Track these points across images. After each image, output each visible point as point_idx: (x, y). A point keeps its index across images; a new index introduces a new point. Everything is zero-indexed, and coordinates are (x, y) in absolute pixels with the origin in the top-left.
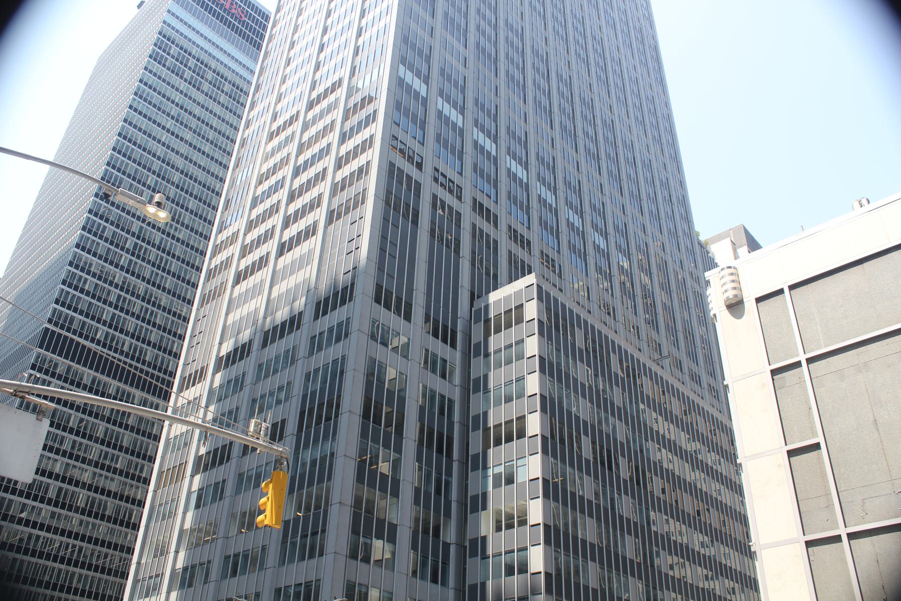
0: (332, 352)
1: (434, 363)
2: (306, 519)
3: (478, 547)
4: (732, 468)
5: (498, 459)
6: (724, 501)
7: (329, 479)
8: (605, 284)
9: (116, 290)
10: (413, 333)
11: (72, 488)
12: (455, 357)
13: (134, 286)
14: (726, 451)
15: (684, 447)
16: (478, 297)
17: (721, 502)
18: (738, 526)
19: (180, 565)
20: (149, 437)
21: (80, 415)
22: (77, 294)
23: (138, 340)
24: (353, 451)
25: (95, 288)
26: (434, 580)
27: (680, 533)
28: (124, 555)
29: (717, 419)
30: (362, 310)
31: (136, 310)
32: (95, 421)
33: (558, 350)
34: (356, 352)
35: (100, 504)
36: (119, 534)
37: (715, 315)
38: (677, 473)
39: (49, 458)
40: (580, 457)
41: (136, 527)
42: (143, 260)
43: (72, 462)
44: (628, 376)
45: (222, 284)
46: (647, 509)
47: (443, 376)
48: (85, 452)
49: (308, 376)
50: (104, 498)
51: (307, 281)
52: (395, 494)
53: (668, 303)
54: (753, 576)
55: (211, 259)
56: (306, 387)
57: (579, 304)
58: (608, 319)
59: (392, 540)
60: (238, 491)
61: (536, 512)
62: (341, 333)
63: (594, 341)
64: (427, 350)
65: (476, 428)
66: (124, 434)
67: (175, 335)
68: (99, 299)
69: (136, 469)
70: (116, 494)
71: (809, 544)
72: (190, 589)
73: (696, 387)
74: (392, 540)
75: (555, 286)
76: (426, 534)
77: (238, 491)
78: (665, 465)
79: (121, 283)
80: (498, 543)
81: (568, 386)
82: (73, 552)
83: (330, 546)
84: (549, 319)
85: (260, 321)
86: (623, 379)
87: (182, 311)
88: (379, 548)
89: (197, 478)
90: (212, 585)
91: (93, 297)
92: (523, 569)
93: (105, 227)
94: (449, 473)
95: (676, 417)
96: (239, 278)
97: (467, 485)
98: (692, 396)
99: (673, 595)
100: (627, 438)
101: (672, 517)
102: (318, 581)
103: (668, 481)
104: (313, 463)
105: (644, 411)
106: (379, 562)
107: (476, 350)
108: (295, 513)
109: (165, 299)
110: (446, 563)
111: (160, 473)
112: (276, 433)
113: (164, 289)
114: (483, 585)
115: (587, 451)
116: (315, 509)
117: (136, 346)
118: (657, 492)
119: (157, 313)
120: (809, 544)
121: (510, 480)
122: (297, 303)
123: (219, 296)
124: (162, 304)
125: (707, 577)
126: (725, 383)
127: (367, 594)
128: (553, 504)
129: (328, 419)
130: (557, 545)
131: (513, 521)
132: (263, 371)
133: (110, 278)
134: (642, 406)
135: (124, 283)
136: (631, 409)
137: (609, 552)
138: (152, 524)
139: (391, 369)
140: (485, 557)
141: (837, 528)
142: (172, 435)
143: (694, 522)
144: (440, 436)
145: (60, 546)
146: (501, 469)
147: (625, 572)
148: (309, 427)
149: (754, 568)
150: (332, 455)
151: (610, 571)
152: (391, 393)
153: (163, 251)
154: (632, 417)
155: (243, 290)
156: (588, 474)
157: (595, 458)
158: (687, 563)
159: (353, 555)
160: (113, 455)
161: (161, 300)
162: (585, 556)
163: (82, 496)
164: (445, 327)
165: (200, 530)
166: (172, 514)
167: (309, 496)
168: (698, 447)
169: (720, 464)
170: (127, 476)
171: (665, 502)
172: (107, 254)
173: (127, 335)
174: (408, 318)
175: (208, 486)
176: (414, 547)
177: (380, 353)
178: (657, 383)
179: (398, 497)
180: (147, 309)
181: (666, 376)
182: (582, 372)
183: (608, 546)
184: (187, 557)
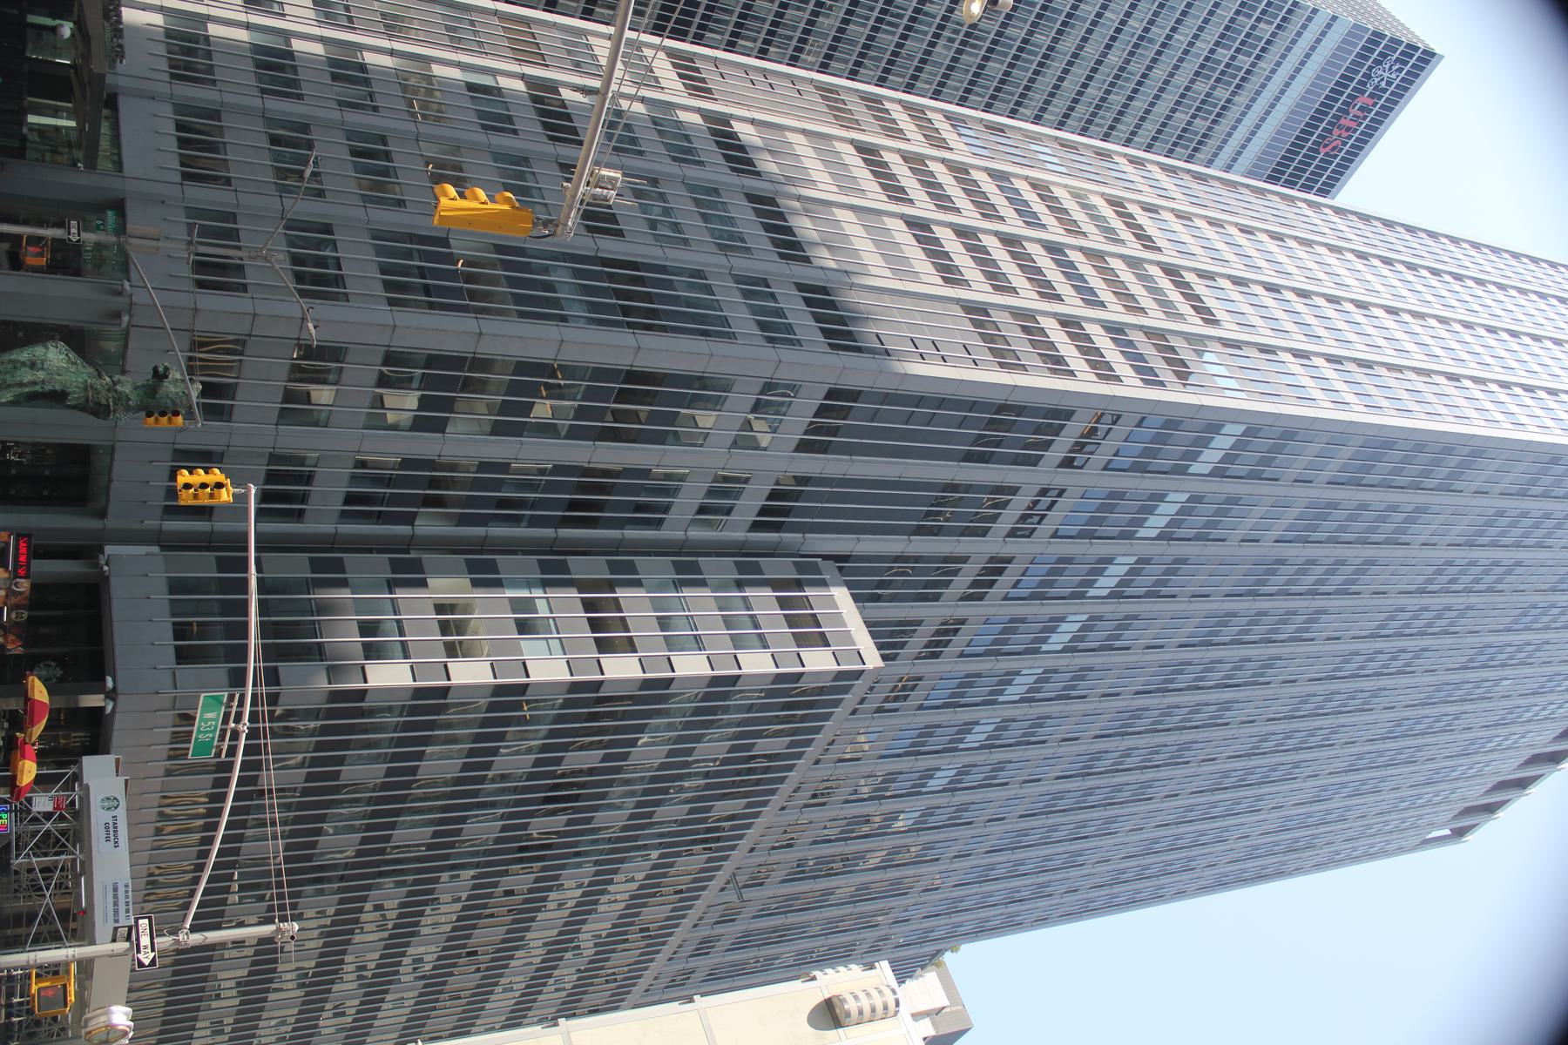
0: (740, 315)
1: (725, 494)
2: (453, 275)
3: (409, 573)
5: (560, 606)
7: (522, 314)
8: (865, 790)
10: (776, 456)
12: (736, 529)
14: (579, 1001)
15: (585, 928)
16: (840, 569)
19: (370, 58)
24: (571, 355)
26: (350, 499)
29: (634, 985)
30: (816, 366)
33: (750, 708)
34: (742, 357)
37: (814, 978)
38: (540, 916)
40: (565, 747)
44: (708, 830)
47: (703, 510)
49: (699, 274)
52: (498, 429)
53: (833, 899)
55: (900, 102)
56: (679, 272)
58: (804, 797)
59: (419, 425)
60: (498, 156)
61: (470, 673)
62: (775, 330)
64: (746, 481)
65: (614, 567)
67: (767, 42)
73: (688, 949)
74: (419, 425)
75: (862, 701)
76: (427, 484)
77: (498, 156)
78: (553, 895)
80: (415, 608)
84: (804, 693)
85: (793, 190)
88: (406, 402)
89: (519, 86)
90: (336, 115)
92: (373, 652)
94: (535, 522)
96: (866, 151)
97: (514, 553)
98: (673, 941)
99: (331, 911)
100: (600, 829)
101: (464, 909)
102: (346, 297)
104: (549, 287)
105: (646, 858)
106: (379, 402)
107: (747, 565)
110: (380, 518)
112: (599, 219)
113: (845, 21)
114: (343, 583)
115: (576, 760)
118: (506, 882)
121: (524, 627)
122: (825, 253)
124: (821, 19)
125: (364, 968)
126: (697, 997)
127: (325, 382)
129: (626, 311)
131: (454, 633)
132: (706, 197)
134: (655, 854)
140: (391, 585)
142: (592, 40)
143: (457, 946)
146: (543, 611)
147: (369, 828)
148: (611, 277)
150: (564, 319)
152: (672, 419)
154: (636, 838)
155: (848, 160)
156: (465, 767)
159: (390, 358)
161: (828, 16)
162: (395, 757)
164: (786, 512)
165: (430, 92)
166: (456, 43)
167: (492, 280)
171: (490, 896)
174: (803, 447)
176: (407, 463)
177: (741, 400)
178: (695, 881)
181: (708, 896)
182: (713, 748)
184: (382, 70)
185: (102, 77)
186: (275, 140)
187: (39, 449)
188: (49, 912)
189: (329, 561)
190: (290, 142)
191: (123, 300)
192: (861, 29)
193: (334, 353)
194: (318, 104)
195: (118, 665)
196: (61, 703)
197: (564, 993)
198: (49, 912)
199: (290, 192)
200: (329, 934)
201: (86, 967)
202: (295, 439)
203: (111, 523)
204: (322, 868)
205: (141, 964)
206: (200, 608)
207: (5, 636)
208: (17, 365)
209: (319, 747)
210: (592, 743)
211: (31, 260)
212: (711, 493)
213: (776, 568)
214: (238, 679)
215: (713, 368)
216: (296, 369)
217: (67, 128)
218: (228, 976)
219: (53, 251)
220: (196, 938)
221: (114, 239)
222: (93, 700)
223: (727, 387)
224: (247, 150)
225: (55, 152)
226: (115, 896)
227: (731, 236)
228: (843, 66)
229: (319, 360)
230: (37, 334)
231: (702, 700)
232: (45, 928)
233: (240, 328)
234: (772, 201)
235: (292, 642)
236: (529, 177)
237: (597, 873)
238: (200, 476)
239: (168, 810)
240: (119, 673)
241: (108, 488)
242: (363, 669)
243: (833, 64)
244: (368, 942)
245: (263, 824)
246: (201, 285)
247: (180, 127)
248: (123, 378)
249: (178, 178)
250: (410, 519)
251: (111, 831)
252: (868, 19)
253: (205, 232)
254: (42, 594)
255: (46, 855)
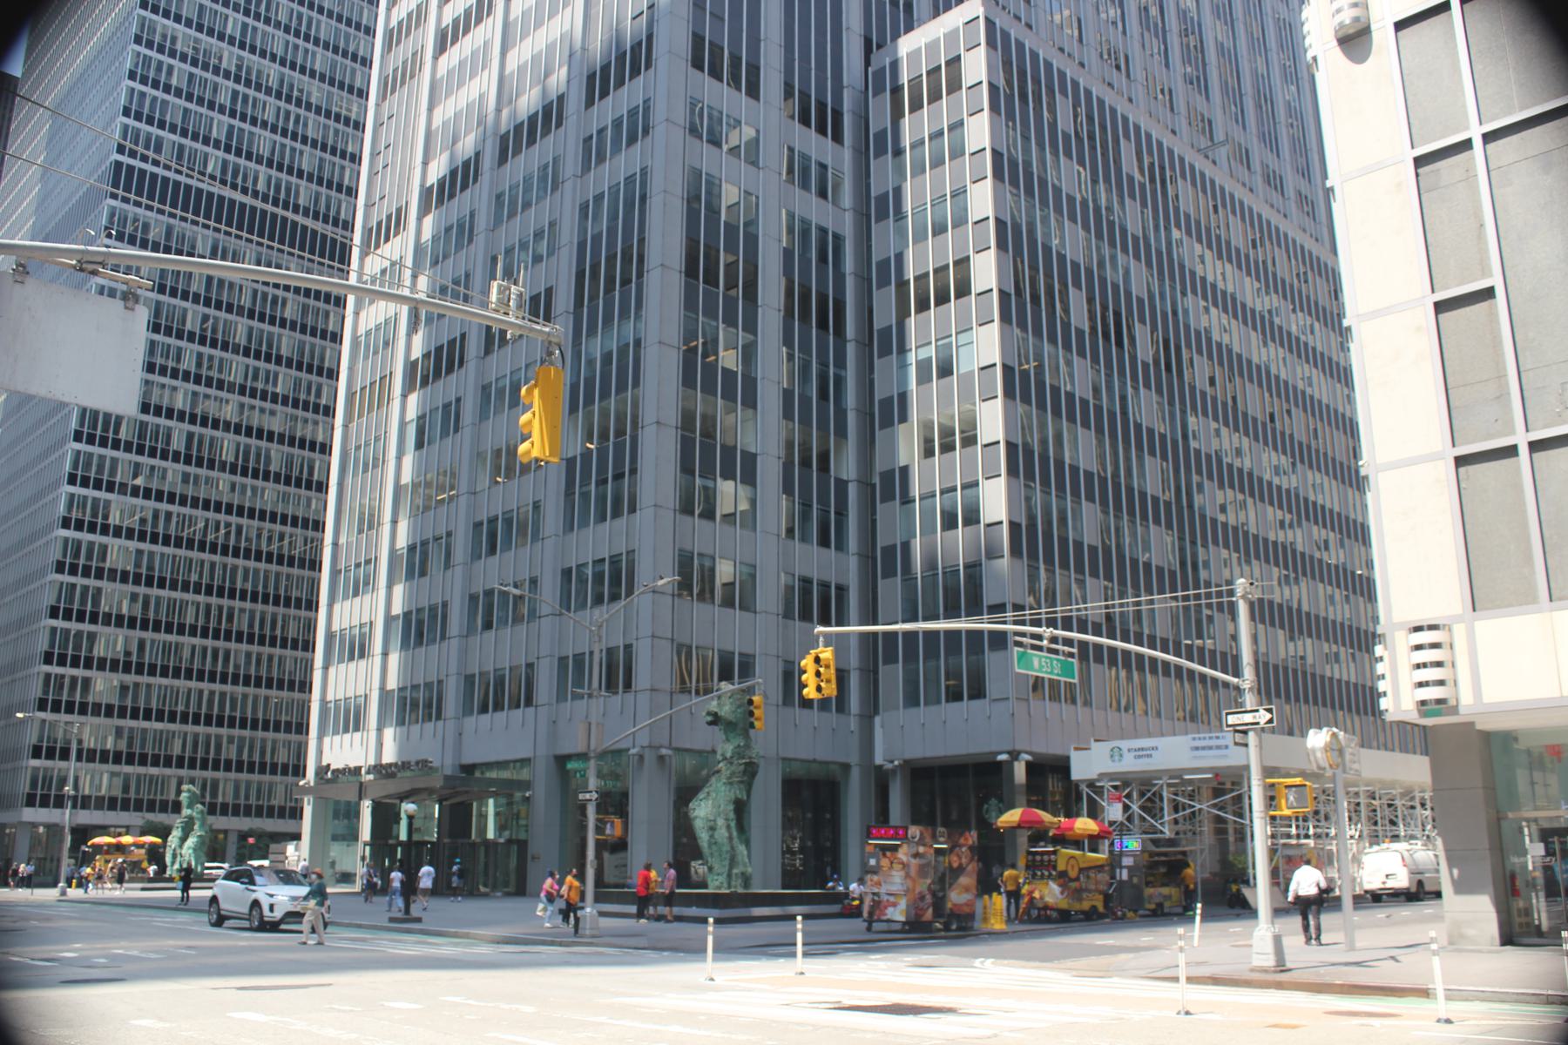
0: (623, 164)
1: (805, 171)
2: (602, 452)
3: (895, 484)
4: (1334, 339)
5: (923, 336)
6: (1317, 396)
7: (636, 383)
8: (1112, 12)
9: (226, 82)
10: (765, 120)
11: (208, 432)
12: (840, 158)
13: (259, 73)
14: (1324, 309)
15: (1249, 304)
16: (879, 47)
17: (1312, 398)
18: (1339, 437)
19: (402, 542)
20: (323, 337)
21: (201, 309)
22: (160, 94)
23: (280, 169)
24: (674, 333)
25: (190, 81)
26: (824, 542)
27: (1239, 452)
28: (310, 533)
29: (1310, 254)
30: (670, 83)
31: (269, 116)
32: (229, 317)
33: (1026, 138)
34: (665, 159)
35: (258, 455)
36: (297, 501)
37: (1315, 59)
38: (1236, 349)
39: (163, 386)
40: (1066, 325)
41: (322, 487)
42: (267, 21)
43: (201, 389)
44: (1152, 180)
45: (415, 54)
46: (1183, 412)
47: (822, 194)
48: (220, 371)
49: (584, 208)
50: (264, 444)
51: (567, 37)
52: (751, 402)
53: (1228, 44)
54: (1360, 520)
55: (389, 10)
56: (583, 230)
57: (1062, 50)
58: (1119, 79)
59: (749, 478)
60: (483, 415)
61: (992, 421)
62: (636, 127)
63: (1090, 119)
64: (791, 150)
65: (884, 282)
66: (280, 336)
67: (343, 155)
68: (200, 101)
69: (309, 393)
70: (281, 437)
71: (1461, 461)
72: (423, 580)
73: (1275, 197)
74: (749, 478)
75: (1018, 18)
76: (807, 468)
77: (483, 415)
78: (1215, 337)
79: (233, 69)
80: (928, 477)
81: (1044, 202)
82: (228, 534)
83: (646, 496)
84: (1009, 82)
85: (491, 118)
86: (1142, 186)
87: (349, 110)
88: (729, 493)
89: (413, 398)
90: (458, 570)
91: (189, 98)
92: (972, 517)
93: (114, 461)
94: (841, 362)
95: (1238, 250)
96: (443, 42)
97: (872, 382)
98: (1267, 213)
99: (1224, 553)
100: (1149, 291)
101: (1226, 424)
102: (630, 553)
103: (1221, 364)
104: (607, 358)
105: (1180, 243)
106: (729, 518)
107: (878, 145)
108: (583, 444)
109: (316, 92)
110: (841, 513)
111: (350, 396)
112: (539, 306)
113: (313, 74)
114: (906, 546)
115: (1079, 316)
116: (616, 436)
117: (248, 447)
118: (1202, 383)
119: (306, 119)
120: (1461, 461)
121: (946, 371)
122: (553, 80)
123: (412, 77)
124: (313, 100)
125: (1282, 523)
126: (1328, 184)
127: (712, 570)
128: (1020, 408)
129: (626, 282)
130: (1030, 476)
131: (954, 438)
132: (506, 206)
133: (213, 61)
134: (1176, 234)
135: (239, 67)
136: (1158, 239)
137: (1117, 486)
138: (349, 480)
139: (730, 187)
140: (907, 500)
141: (1512, 432)
142: (362, 330)
143: (1265, 432)
144: (822, 300)
145: (206, 526)
146: (931, 352)
147: (1144, 517)
148: (594, 297)
149: (1365, 507)
150: (638, 343)
151: (1118, 517)
152: (731, 229)
153: (289, 100)
154: (1159, 253)
155: (455, 61)
156: (1086, 425)
157: (1093, 329)
158: (1250, 501)
159: (687, 508)
160: (268, 372)
161: (309, 94)
162: (1076, 493)
163: (228, 445)
164: (822, 106)
165: (428, 485)
166: (378, 462)
167: (604, 414)
168: (1275, 304)
169: (1312, 332)
170: (296, 405)
171: (1214, 399)
172: (200, 16)
173: (259, 162)
174: (753, 92)
175: (433, 411)
176: (788, 489)
177: (707, 159)
178: (1204, 191)
179: (754, 407)
180: (288, 113)
181: (1221, 178)
182: (1069, 176)
183: (1116, 475)
184: (413, 530)
185: (447, 778)
186: (488, 625)
187: (788, 824)
188: (1214, 806)
189: (884, 560)
190: (489, 610)
191: (648, 755)
192: (319, 57)
193: (685, 563)
194: (451, 586)
195: (986, 749)
196: (1022, 799)
197: (1316, 325)
198: (1214, 806)
199: (535, 610)
200: (1247, 553)
201: (1268, 772)
202: (769, 596)
203: (854, 759)
204: (1183, 564)
205: (1270, 721)
206: (932, 680)
207: (961, 846)
208: (713, 842)
209: (1065, 565)
210: (1061, 301)
211: (618, 832)
212: (805, 185)
213: (880, 117)
214: (999, 640)
215: (678, 189)
216: (701, 597)
217: (496, 806)
218: (1284, 648)
219: (607, 813)
220: (1248, 673)
221: (592, 763)
222: (1020, 772)
223: (697, 174)
224: (501, 650)
225: (518, 816)
226: (1204, 748)
227: (543, 179)
228: (359, 74)
229: (693, 578)
230: (683, 828)
231: (1018, 187)
232: (1230, 808)
233: (666, 652)
234: (504, 139)
235: (965, 591)
236: (500, 384)
237: (1194, 292)
238: (809, 677)
239: (1123, 702)
240: (994, 748)
241: (821, 763)
242: (989, 525)
243: (358, 84)
244: (1259, 518)
245: (1138, 614)
246: (628, 685)
247: (484, 709)
248: (719, 752)
249: (531, 710)
250: (843, 489)
251: (1141, 753)
252: (307, 51)
253: (578, 683)
254: (919, 815)
255: (1162, 809)
